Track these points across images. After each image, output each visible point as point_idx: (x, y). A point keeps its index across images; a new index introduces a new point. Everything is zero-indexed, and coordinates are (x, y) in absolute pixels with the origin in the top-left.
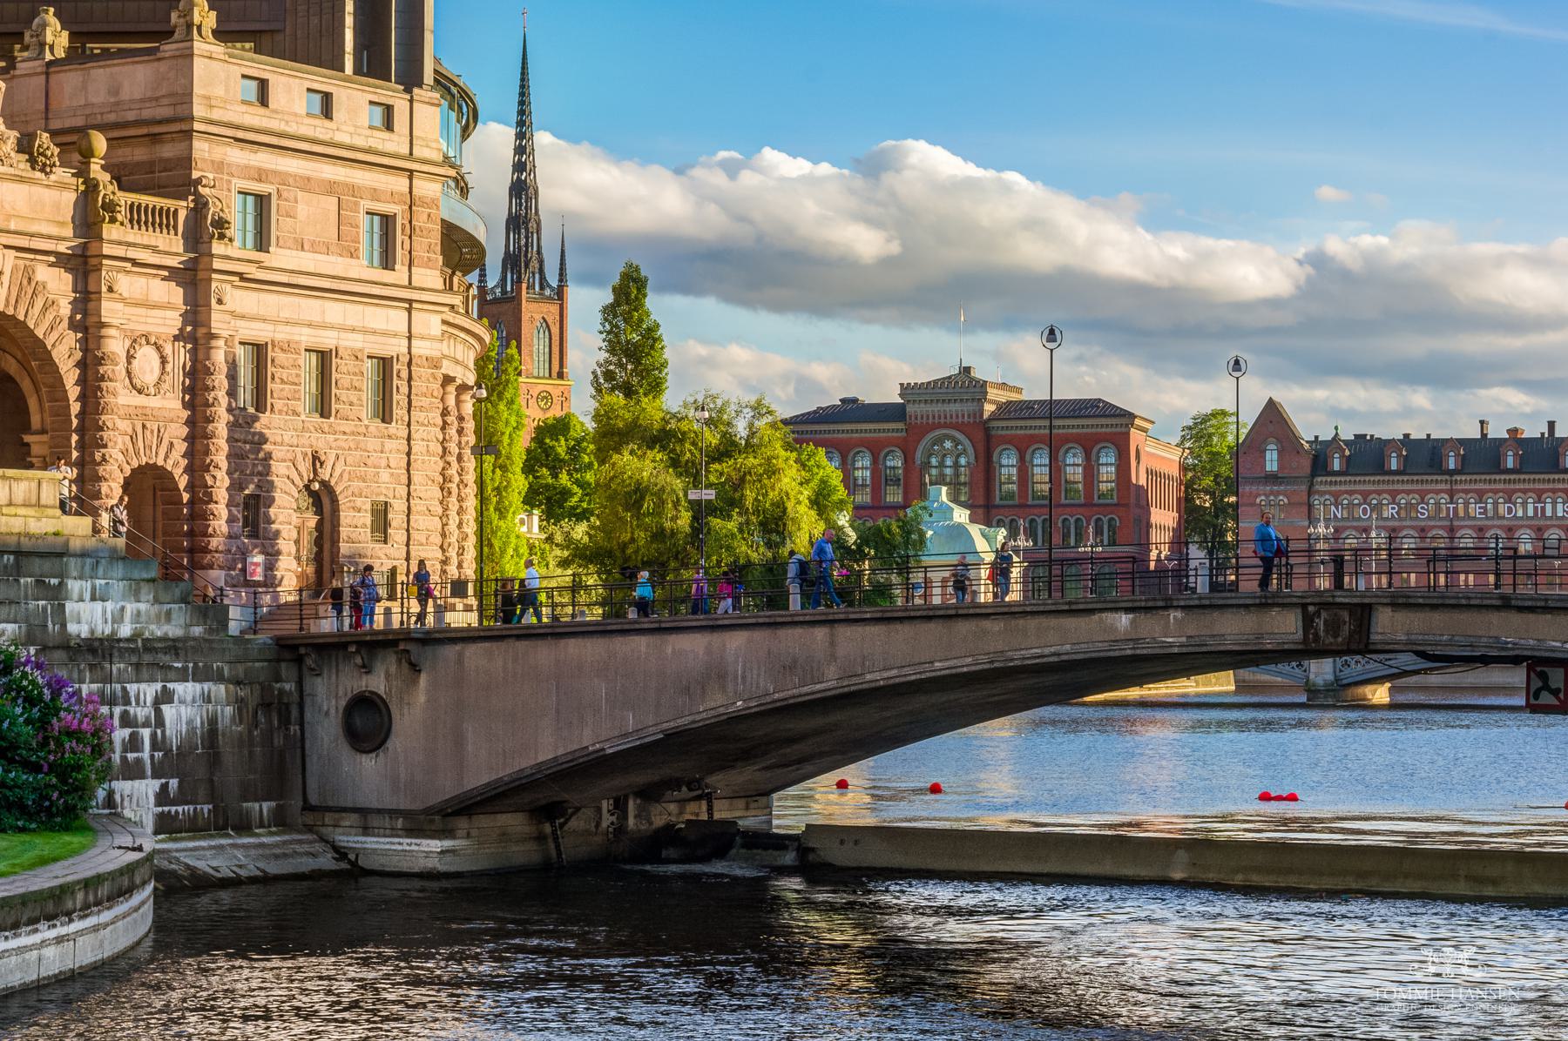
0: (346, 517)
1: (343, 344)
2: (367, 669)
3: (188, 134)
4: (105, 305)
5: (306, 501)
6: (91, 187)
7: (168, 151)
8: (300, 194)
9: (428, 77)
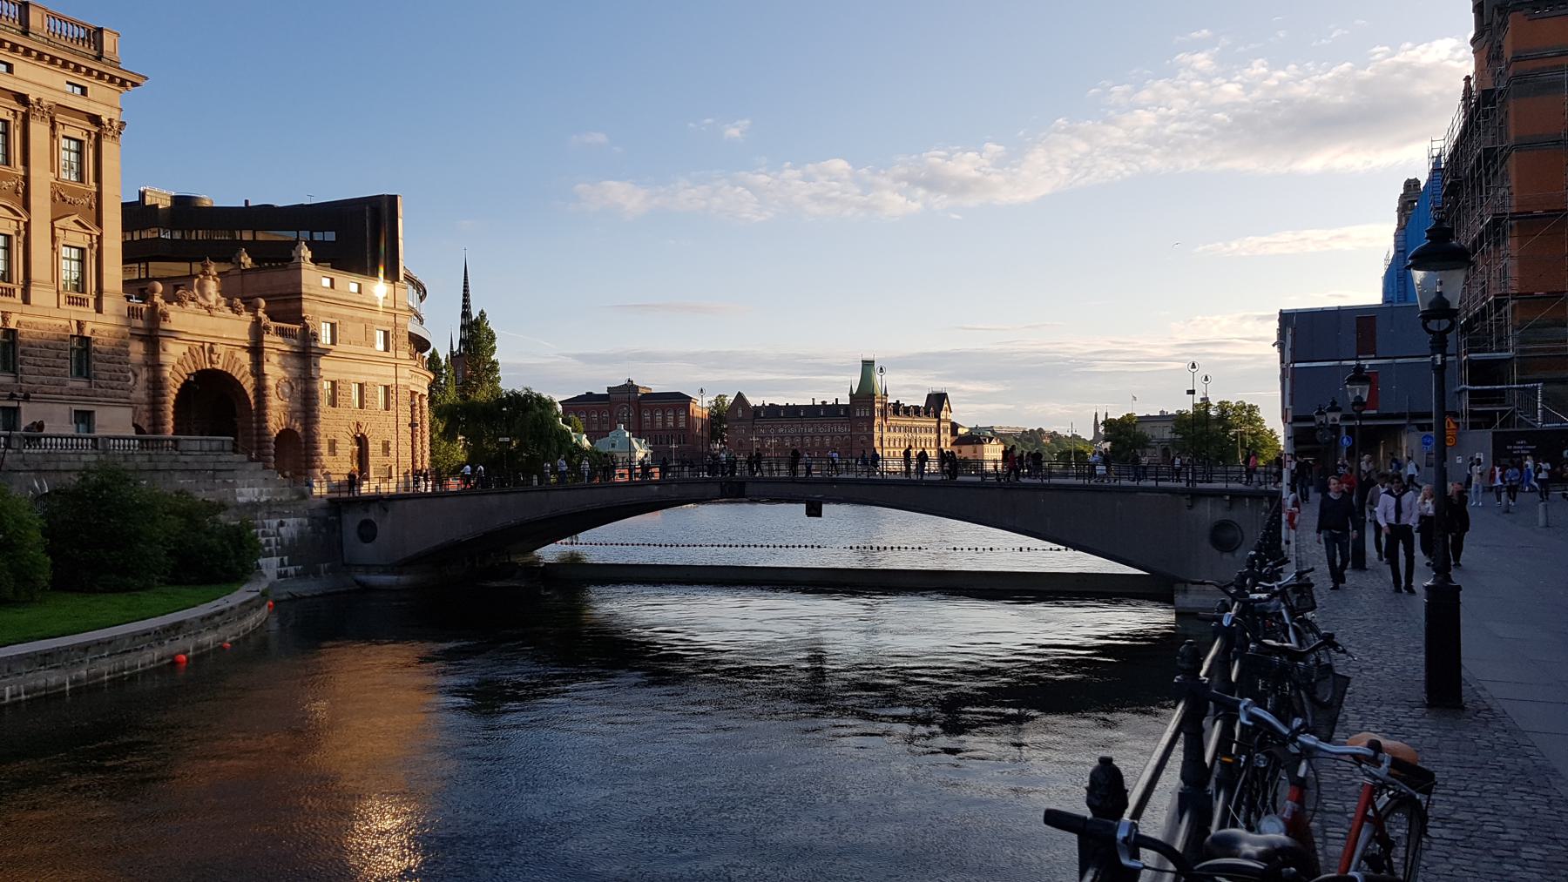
0: (371, 446)
1: (368, 381)
2: (367, 511)
3: (300, 299)
4: (265, 367)
5: (354, 441)
6: (259, 320)
7: (292, 306)
8: (349, 323)
9: (401, 277)
